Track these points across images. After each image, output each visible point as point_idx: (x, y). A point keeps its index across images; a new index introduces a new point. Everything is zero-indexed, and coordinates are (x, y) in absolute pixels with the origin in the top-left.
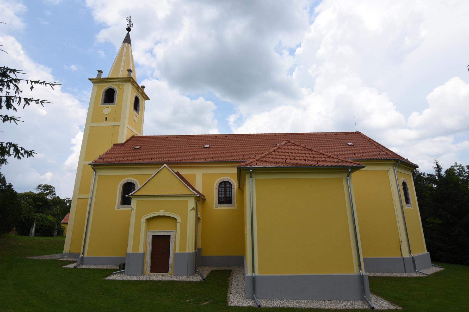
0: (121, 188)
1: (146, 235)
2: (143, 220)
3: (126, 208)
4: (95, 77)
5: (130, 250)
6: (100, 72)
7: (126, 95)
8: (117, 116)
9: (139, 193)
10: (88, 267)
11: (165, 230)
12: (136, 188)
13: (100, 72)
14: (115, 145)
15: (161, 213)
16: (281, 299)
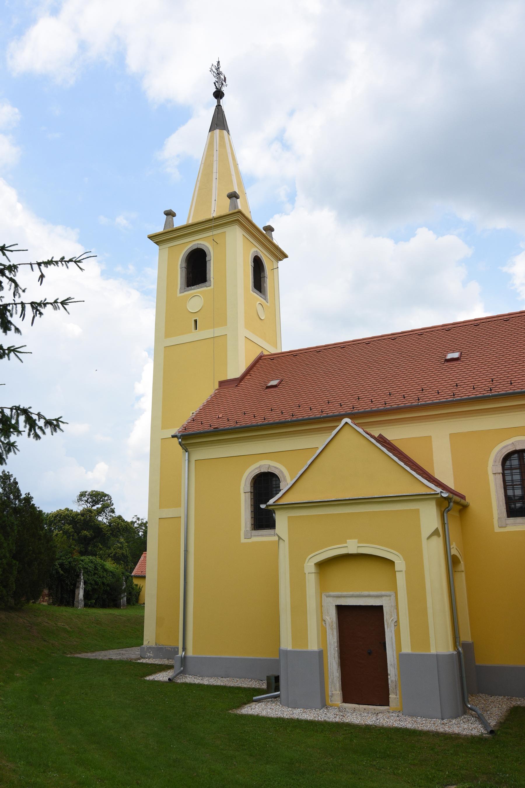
0: (248, 489)
2: (310, 566)
3: (264, 537)
4: (160, 229)
5: (287, 644)
6: (170, 214)
7: (231, 257)
8: (219, 315)
9: (288, 499)
11: (366, 593)
12: (282, 485)
13: (170, 214)
15: (352, 547)
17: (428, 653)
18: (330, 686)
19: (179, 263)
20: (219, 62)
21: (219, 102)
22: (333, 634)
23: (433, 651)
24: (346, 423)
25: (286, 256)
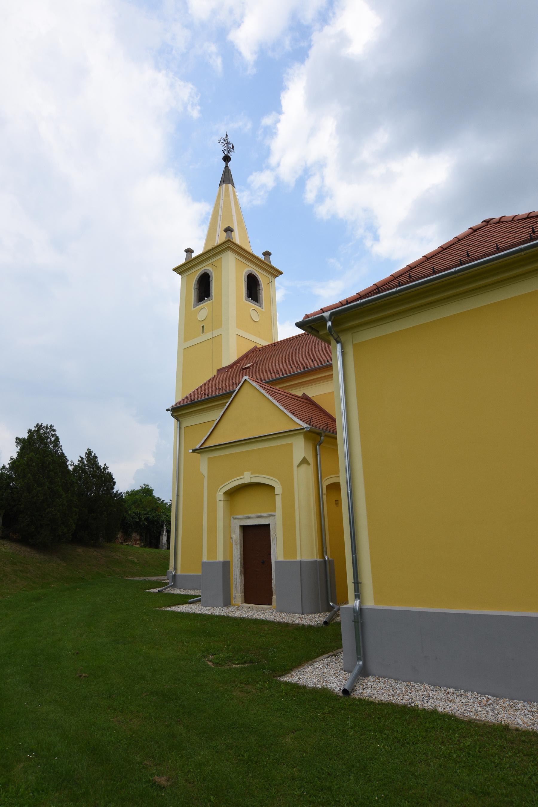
1: (228, 528)
2: (220, 496)
4: (182, 261)
6: (189, 251)
7: (230, 277)
8: (216, 320)
10: (183, 592)
11: (259, 514)
13: (189, 251)
14: (219, 371)
15: (247, 478)
16: (436, 685)
17: (295, 560)
18: (234, 590)
19: (193, 286)
20: (227, 135)
21: (227, 164)
22: (237, 549)
23: (299, 559)
24: (246, 380)
25: (281, 273)
